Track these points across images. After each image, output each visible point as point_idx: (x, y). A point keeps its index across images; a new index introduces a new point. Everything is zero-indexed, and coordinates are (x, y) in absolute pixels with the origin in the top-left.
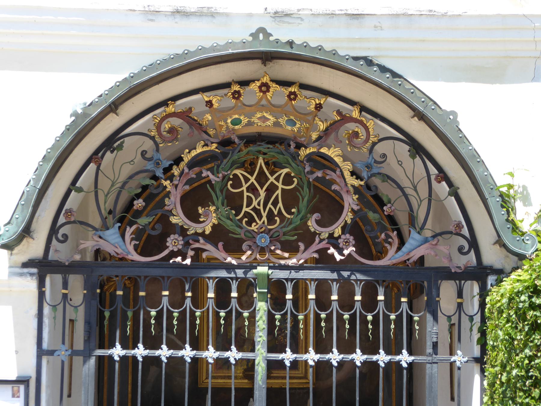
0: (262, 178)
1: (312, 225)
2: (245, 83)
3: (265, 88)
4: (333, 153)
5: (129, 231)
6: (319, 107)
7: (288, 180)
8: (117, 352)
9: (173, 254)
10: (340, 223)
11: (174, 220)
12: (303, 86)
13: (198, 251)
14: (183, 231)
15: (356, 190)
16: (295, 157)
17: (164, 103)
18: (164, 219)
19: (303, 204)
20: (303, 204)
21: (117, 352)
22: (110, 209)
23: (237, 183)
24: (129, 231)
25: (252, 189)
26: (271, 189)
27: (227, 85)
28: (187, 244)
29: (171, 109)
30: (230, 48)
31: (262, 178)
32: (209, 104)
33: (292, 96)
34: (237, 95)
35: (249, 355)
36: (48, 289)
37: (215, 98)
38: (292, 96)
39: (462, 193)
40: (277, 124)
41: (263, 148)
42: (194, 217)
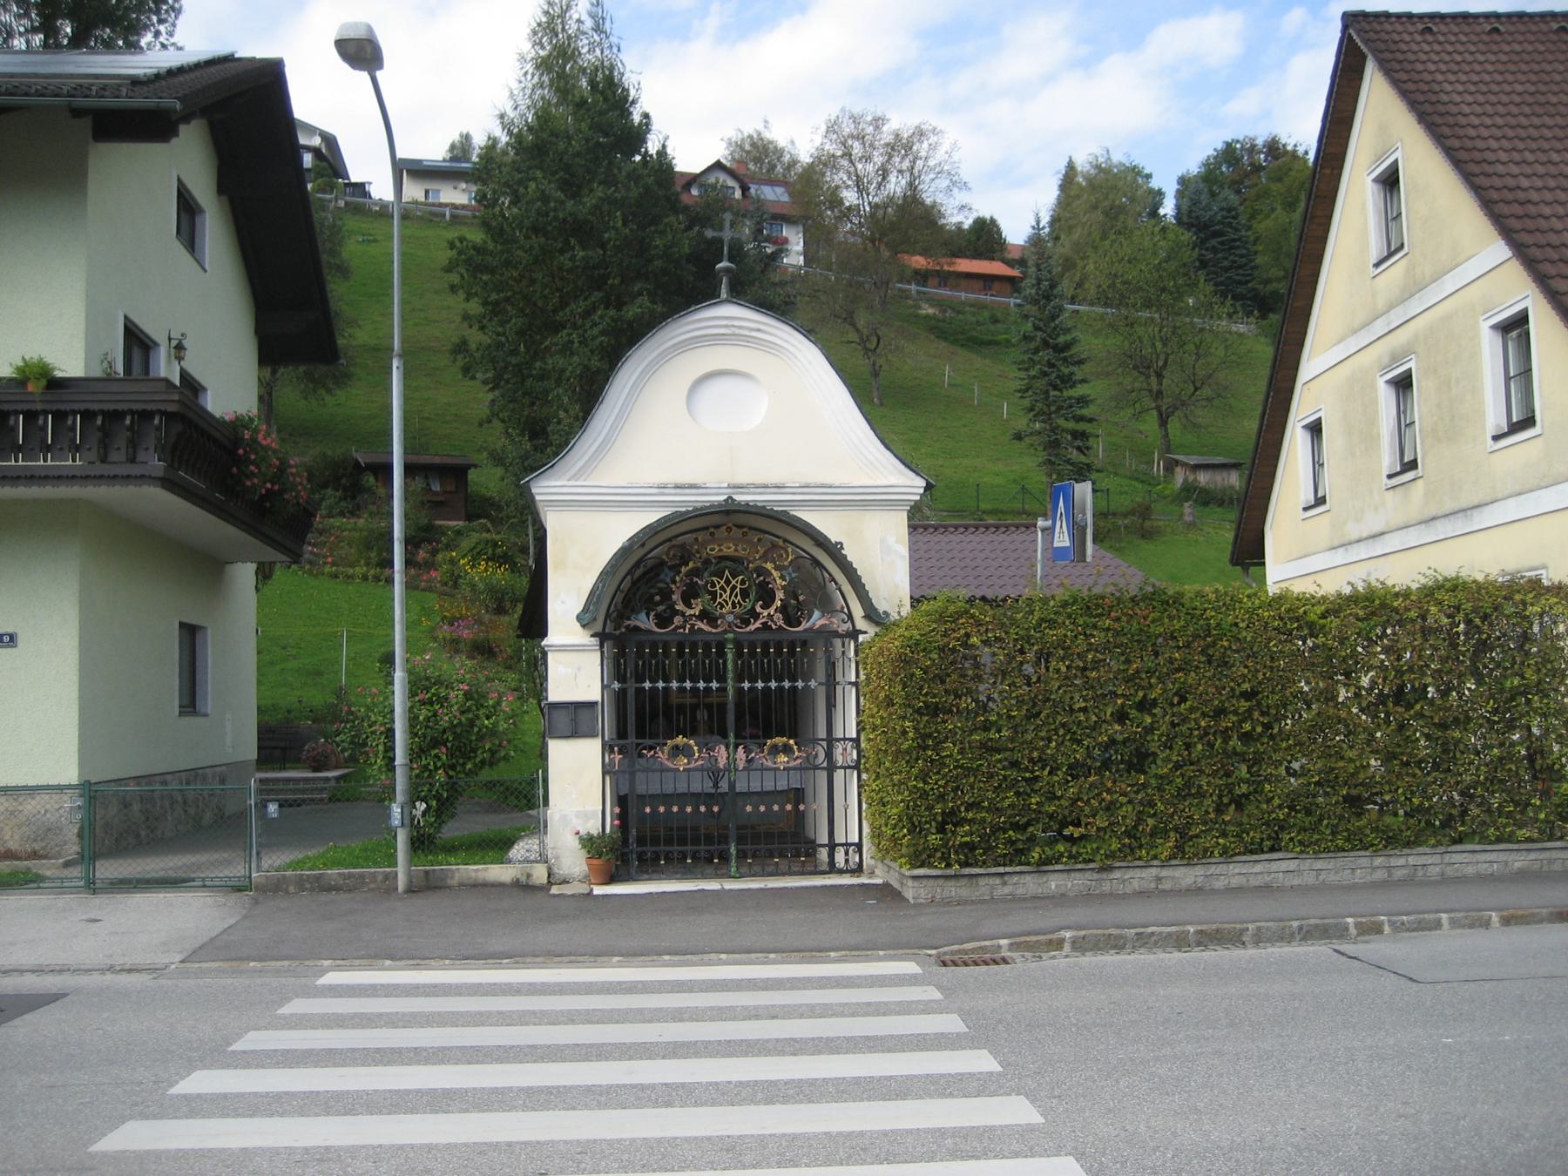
0: (728, 582)
1: (758, 609)
2: (717, 527)
3: (729, 530)
4: (769, 566)
5: (652, 614)
6: (759, 540)
7: (743, 582)
8: (647, 685)
9: (677, 627)
10: (774, 607)
11: (677, 607)
12: (751, 528)
13: (693, 626)
14: (683, 614)
15: (783, 587)
16: (747, 568)
17: (670, 540)
18: (672, 607)
19: (753, 596)
20: (753, 596)
21: (647, 685)
22: (467, 138)
23: (713, 585)
24: (652, 614)
25: (722, 588)
26: (734, 587)
27: (707, 528)
28: (685, 621)
29: (674, 542)
30: (1164, 230)
31: (728, 582)
32: (696, 539)
33: (745, 534)
34: (712, 534)
35: (724, 685)
36: (605, 649)
37: (701, 536)
38: (745, 534)
39: (843, 588)
40: (720, 550)
41: (729, 563)
42: (689, 606)
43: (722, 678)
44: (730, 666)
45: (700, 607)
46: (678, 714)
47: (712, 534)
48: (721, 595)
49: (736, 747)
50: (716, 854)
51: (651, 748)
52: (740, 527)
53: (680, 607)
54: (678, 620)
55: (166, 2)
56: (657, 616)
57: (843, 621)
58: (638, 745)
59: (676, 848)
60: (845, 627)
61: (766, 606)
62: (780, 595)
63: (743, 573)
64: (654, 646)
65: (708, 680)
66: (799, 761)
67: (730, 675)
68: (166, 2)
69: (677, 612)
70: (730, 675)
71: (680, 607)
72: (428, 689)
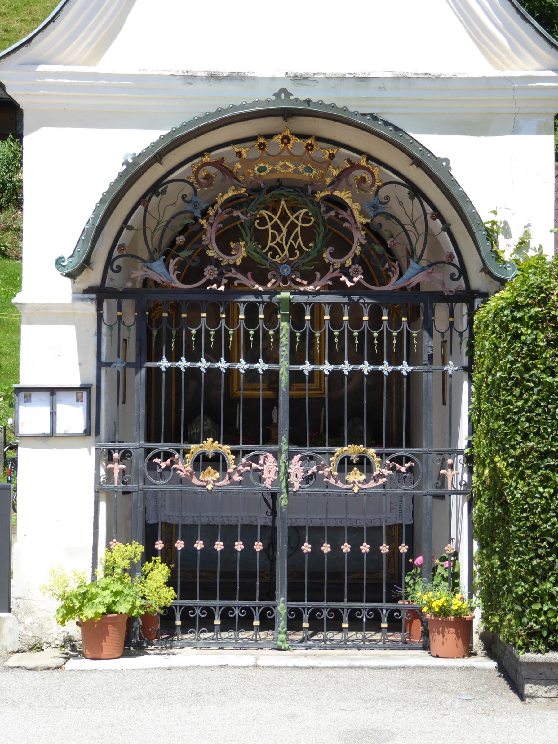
0: (284, 218)
1: (326, 256)
2: (269, 137)
3: (286, 140)
5: (173, 263)
6: (332, 156)
7: (305, 220)
8: (164, 364)
10: (351, 255)
11: (210, 253)
12: (319, 139)
17: (201, 154)
18: (203, 254)
19: (319, 239)
20: (319, 239)
21: (164, 364)
23: (263, 221)
25: (276, 227)
26: (293, 226)
27: (254, 139)
28: (221, 274)
29: (207, 159)
31: (284, 218)
32: (239, 154)
33: (309, 147)
34: (262, 147)
35: (274, 367)
37: (244, 149)
38: (309, 147)
39: (453, 229)
42: (227, 251)
43: (271, 358)
44: (284, 340)
45: (244, 253)
46: (342, 349)
47: (262, 147)
48: (274, 238)
49: (290, 456)
50: (257, 615)
51: (167, 455)
52: (303, 136)
53: (213, 252)
54: (210, 272)
55: (1, 204)
56: (180, 266)
57: (452, 276)
58: (148, 451)
59: (198, 602)
60: (454, 286)
61: (340, 253)
62: (359, 237)
63: (306, 205)
64: (176, 308)
65: (252, 358)
66: (381, 481)
67: (284, 351)
68: (1, 204)
69: (209, 261)
70: (284, 351)
71: (213, 252)
72: (523, 561)
